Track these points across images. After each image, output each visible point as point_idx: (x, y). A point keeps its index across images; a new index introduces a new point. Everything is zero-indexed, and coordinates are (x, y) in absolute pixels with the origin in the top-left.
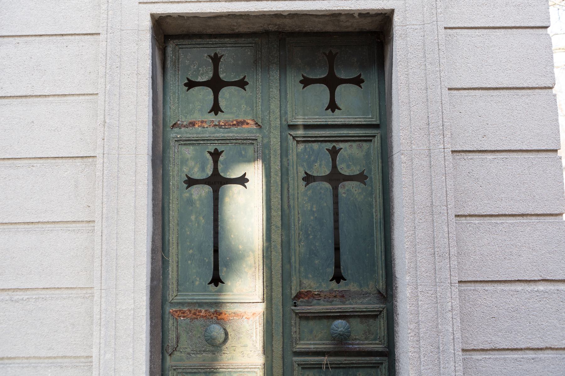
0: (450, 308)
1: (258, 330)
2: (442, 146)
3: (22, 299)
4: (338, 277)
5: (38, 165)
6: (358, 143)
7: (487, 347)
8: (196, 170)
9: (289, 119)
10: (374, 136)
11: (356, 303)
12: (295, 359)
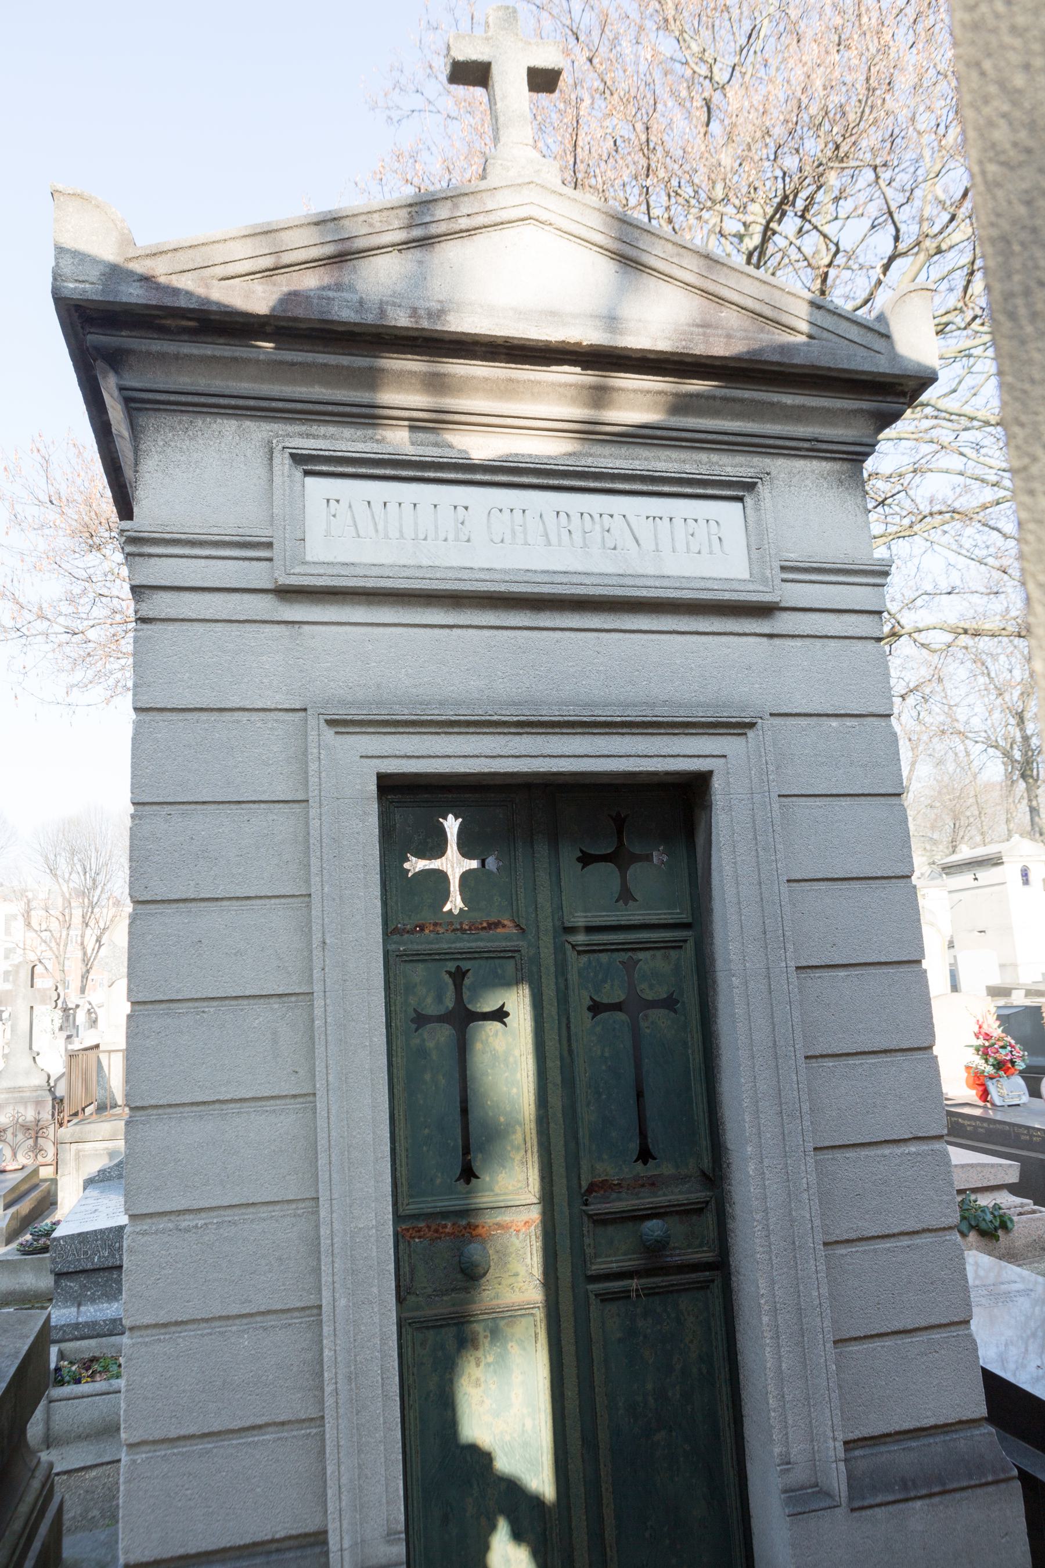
0: (805, 1186)
1: (534, 1248)
2: (783, 964)
3: (196, 1227)
4: (645, 1155)
5: (212, 1010)
6: (663, 951)
7: (853, 1235)
8: (429, 1000)
9: (566, 918)
10: (685, 941)
11: (673, 1193)
12: (590, 1287)
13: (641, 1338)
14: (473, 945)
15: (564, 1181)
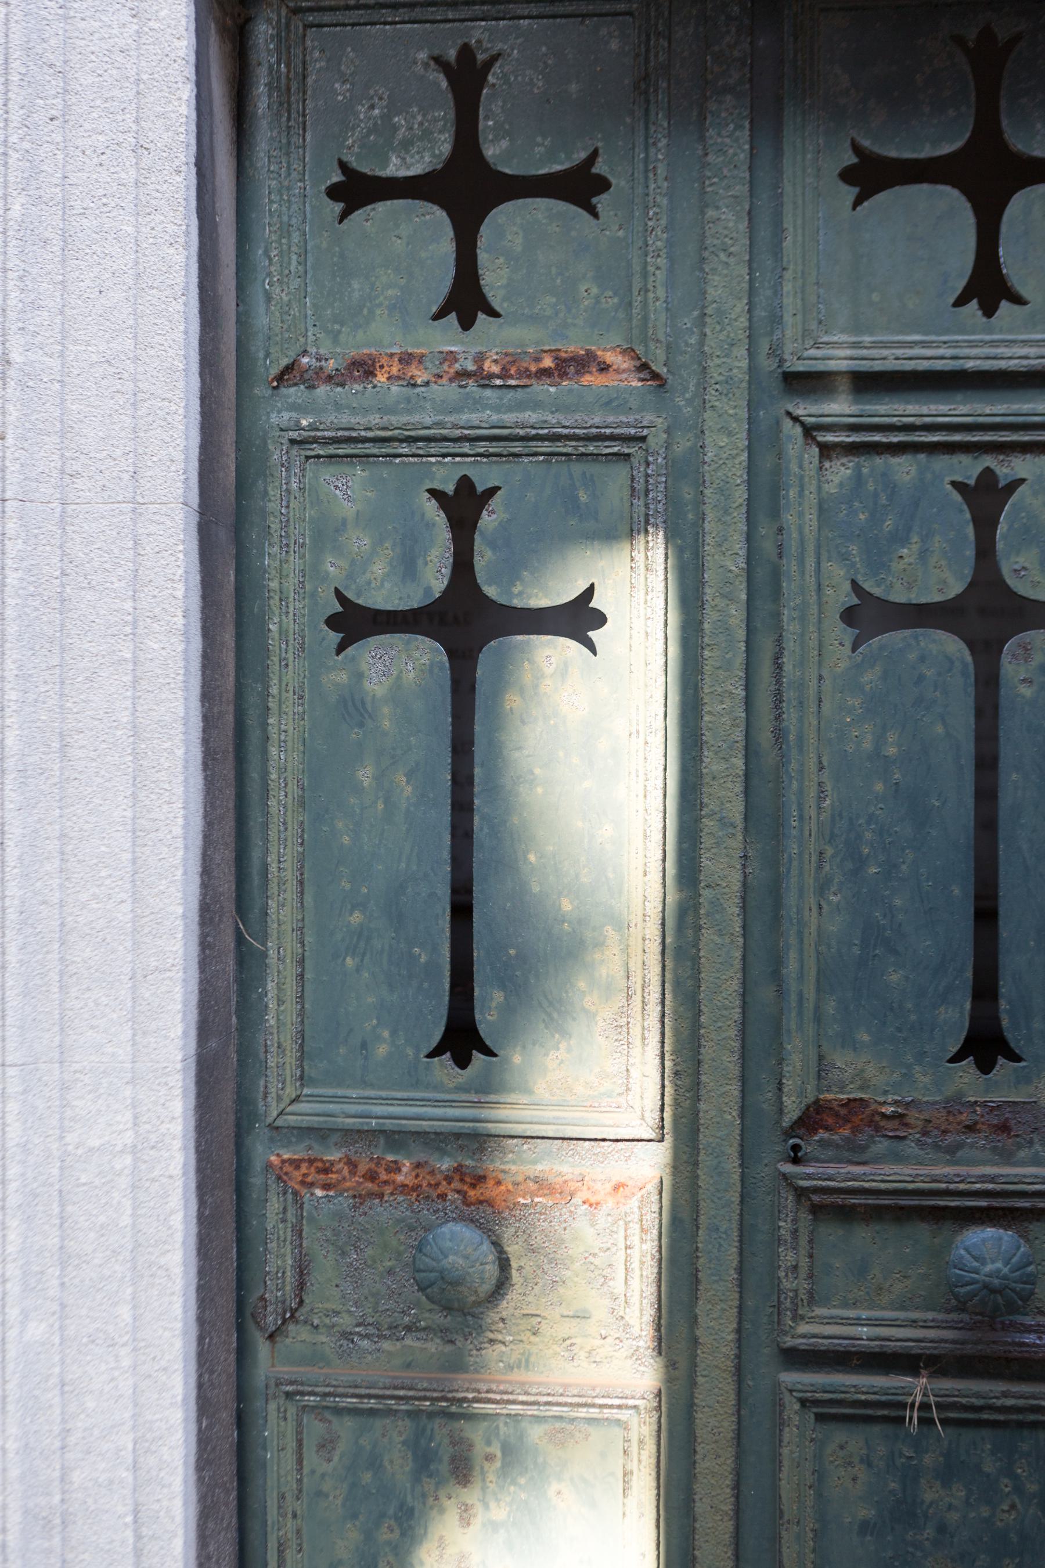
1: (636, 1254)
4: (985, 1045)
8: (379, 569)
12: (790, 1378)
13: (929, 1532)
14: (509, 418)
15: (734, 1089)
